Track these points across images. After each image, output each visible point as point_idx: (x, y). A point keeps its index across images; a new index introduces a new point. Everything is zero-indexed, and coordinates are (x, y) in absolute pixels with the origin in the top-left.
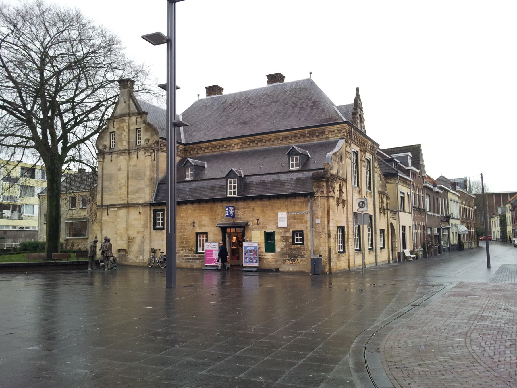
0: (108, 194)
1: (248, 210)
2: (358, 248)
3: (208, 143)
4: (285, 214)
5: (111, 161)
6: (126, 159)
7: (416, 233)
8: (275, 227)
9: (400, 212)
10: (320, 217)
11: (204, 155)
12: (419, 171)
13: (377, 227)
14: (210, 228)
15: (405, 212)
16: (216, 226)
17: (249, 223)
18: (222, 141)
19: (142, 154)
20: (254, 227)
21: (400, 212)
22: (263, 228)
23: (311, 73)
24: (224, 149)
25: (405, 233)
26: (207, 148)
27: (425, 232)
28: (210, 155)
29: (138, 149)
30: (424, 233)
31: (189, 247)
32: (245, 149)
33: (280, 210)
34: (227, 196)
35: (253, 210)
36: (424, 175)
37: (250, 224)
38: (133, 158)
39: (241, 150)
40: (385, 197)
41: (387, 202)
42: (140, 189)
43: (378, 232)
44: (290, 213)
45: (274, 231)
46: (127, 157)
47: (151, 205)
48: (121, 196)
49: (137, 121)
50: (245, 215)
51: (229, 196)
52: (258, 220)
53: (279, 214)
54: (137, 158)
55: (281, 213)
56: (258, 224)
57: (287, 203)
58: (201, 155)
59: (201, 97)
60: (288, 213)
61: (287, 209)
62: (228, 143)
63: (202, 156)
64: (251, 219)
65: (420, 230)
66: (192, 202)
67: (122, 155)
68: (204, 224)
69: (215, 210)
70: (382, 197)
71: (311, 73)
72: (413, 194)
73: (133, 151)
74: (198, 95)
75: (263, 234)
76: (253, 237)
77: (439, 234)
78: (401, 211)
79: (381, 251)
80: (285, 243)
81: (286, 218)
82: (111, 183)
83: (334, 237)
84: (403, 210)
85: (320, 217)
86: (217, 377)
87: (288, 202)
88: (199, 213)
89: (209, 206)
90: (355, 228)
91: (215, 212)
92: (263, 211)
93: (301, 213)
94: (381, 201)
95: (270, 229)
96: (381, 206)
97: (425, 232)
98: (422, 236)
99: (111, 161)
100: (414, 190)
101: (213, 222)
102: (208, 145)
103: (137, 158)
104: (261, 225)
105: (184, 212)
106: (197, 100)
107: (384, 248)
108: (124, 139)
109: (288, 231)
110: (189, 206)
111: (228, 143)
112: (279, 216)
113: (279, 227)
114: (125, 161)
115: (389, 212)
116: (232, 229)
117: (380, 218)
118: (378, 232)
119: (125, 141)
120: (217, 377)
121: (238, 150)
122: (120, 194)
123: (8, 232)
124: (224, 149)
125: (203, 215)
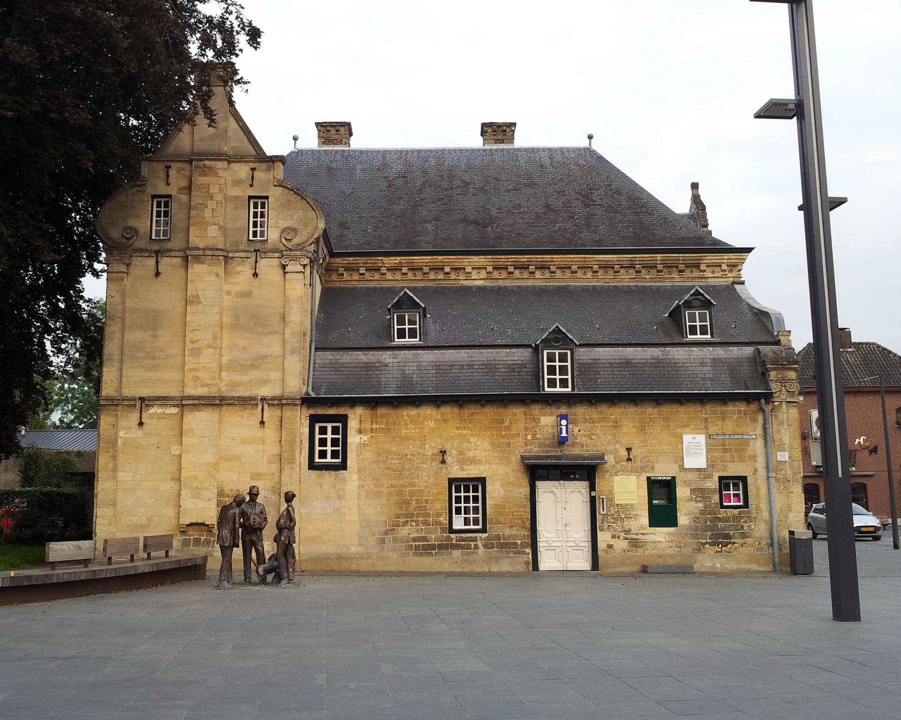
0: (142, 367)
1: (602, 426)
4: (701, 439)
5: (157, 274)
6: (217, 275)
14: (494, 467)
18: (440, 257)
22: (643, 469)
24: (441, 276)
26: (393, 269)
31: (428, 515)
32: (500, 281)
33: (687, 429)
35: (616, 425)
37: (610, 459)
38: (238, 273)
39: (488, 283)
42: (263, 357)
44: (715, 437)
46: (220, 270)
47: (307, 401)
48: (197, 374)
49: (253, 177)
50: (594, 437)
51: (548, 390)
52: (629, 450)
53: (687, 438)
54: (255, 275)
55: (692, 436)
56: (629, 459)
59: (302, 145)
60: (709, 436)
61: (706, 428)
64: (610, 448)
69: (507, 424)
76: (616, 490)
80: (700, 505)
85: (786, 447)
88: (458, 428)
89: (490, 412)
93: (740, 437)
95: (662, 472)
99: (157, 274)
103: (255, 275)
104: (638, 463)
109: (710, 477)
110: (428, 411)
112: (685, 443)
114: (214, 278)
119: (214, 224)
121: (482, 282)
122: (196, 370)
125: (472, 435)
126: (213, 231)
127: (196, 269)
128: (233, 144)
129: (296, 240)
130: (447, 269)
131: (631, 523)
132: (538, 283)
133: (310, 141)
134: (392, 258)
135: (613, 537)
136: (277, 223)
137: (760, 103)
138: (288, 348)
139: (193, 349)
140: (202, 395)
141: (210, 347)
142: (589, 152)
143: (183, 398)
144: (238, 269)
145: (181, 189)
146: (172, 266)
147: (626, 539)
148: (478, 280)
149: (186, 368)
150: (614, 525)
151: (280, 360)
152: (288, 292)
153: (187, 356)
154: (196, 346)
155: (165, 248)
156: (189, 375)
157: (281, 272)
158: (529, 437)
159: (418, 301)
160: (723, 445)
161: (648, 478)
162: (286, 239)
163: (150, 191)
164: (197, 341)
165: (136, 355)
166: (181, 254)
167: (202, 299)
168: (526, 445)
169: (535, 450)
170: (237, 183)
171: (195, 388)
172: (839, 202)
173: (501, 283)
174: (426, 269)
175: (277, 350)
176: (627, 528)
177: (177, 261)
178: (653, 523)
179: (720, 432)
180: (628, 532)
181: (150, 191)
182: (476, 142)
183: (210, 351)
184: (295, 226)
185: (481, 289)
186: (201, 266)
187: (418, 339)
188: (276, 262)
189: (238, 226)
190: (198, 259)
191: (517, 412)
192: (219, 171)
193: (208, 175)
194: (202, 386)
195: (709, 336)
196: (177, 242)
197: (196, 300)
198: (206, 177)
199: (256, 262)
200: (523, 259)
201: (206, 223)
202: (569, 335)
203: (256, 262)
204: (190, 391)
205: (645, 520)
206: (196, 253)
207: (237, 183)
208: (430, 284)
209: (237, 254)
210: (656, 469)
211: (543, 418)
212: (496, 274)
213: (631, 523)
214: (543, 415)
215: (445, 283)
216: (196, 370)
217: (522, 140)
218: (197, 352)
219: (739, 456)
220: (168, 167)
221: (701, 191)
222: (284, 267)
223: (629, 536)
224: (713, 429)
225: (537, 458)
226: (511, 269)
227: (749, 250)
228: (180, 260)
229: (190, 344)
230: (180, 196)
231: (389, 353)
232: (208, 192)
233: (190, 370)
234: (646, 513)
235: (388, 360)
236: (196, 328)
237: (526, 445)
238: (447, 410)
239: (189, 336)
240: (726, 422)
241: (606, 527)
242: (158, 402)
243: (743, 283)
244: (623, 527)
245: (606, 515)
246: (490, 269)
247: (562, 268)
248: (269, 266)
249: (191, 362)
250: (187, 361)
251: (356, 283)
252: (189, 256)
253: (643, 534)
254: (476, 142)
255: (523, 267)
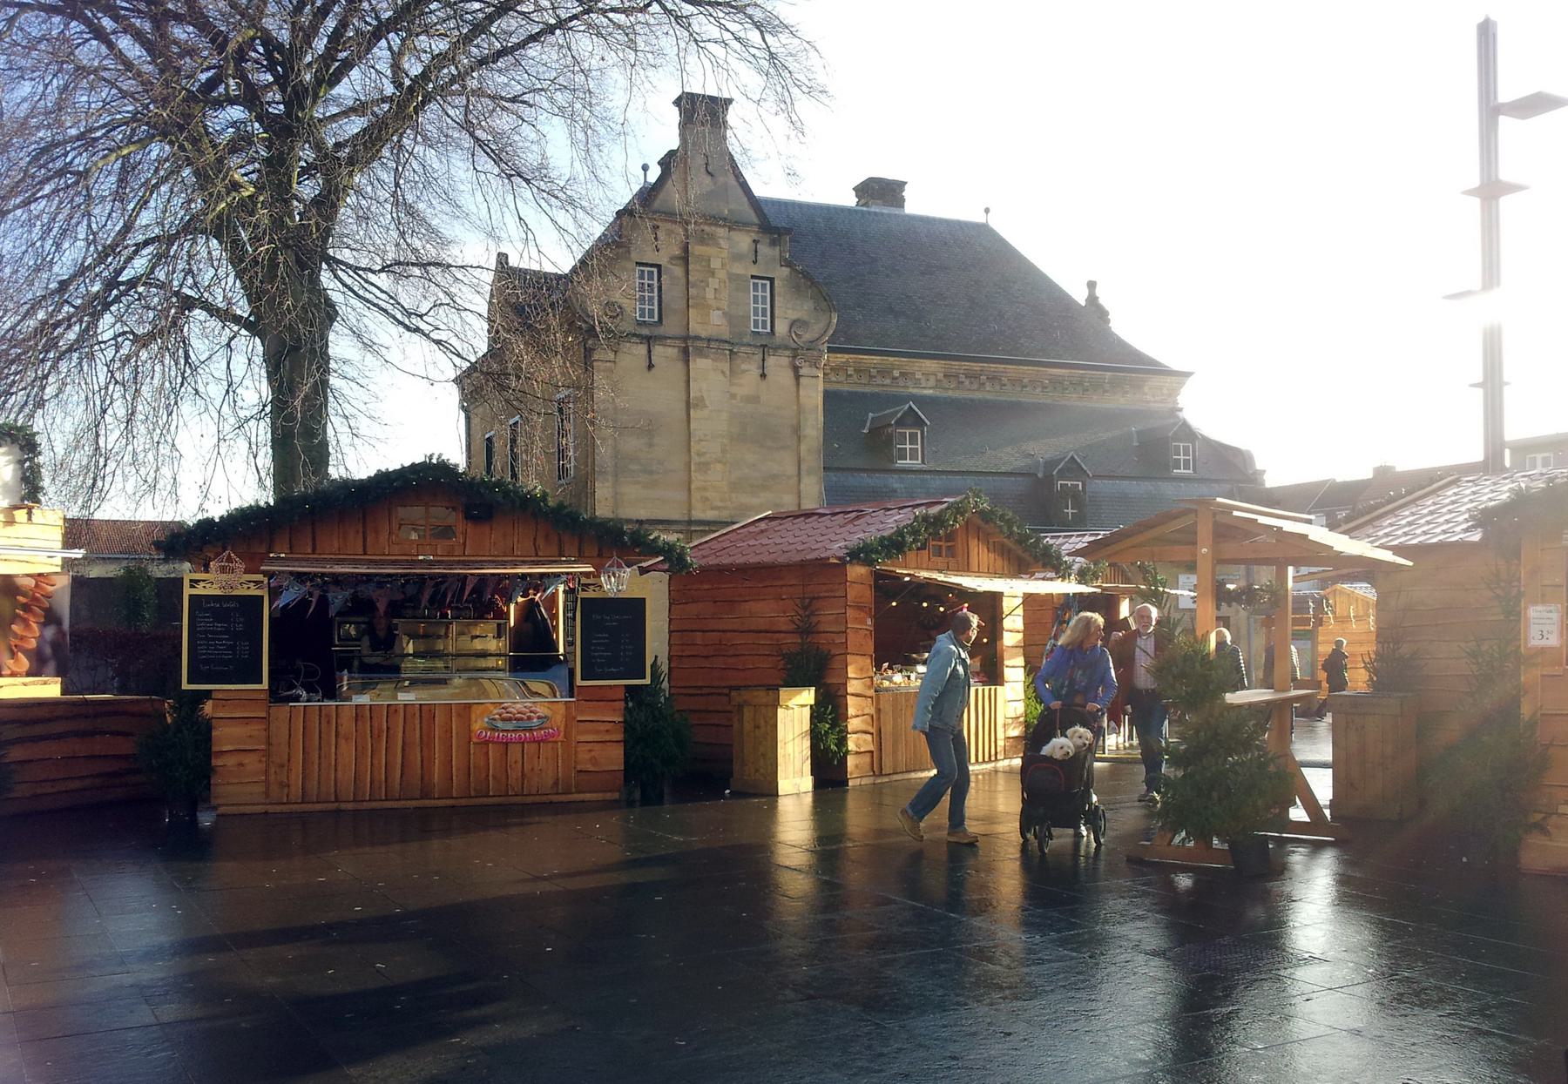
0: (639, 483)
3: (846, 356)
5: (650, 366)
6: (723, 372)
18: (891, 359)
19: (781, 366)
23: (987, 211)
24: (888, 381)
29: (766, 346)
38: (744, 372)
42: (774, 477)
46: (726, 366)
48: (708, 494)
49: (756, 252)
54: (763, 376)
55: (1187, 576)
62: (908, 369)
67: (706, 357)
71: (987, 211)
73: (749, 350)
82: (651, 445)
86: (1069, 947)
99: (650, 366)
102: (847, 361)
103: (763, 376)
108: (713, 303)
113: (1180, 607)
114: (721, 377)
119: (718, 309)
120: (1069, 947)
121: (931, 391)
122: (705, 489)
124: (888, 381)
126: (716, 318)
127: (700, 364)
128: (732, 207)
129: (808, 336)
130: (896, 373)
132: (989, 397)
134: (839, 355)
136: (785, 312)
138: (804, 467)
139: (700, 463)
140: (712, 519)
141: (719, 462)
142: (983, 230)
143: (690, 522)
144: (744, 367)
145: (673, 258)
146: (667, 357)
149: (693, 487)
151: (794, 481)
152: (802, 400)
153: (695, 471)
154: (702, 460)
155: (656, 333)
156: (696, 495)
157: (791, 374)
159: (923, 417)
162: (796, 334)
163: (635, 256)
164: (705, 453)
165: (631, 467)
166: (678, 343)
167: (707, 403)
170: (737, 257)
171: (704, 511)
172: (1507, 384)
175: (791, 469)
177: (672, 352)
181: (635, 256)
182: (850, 200)
183: (719, 467)
184: (806, 318)
186: (704, 361)
187: (920, 462)
188: (785, 361)
189: (741, 314)
190: (701, 353)
192: (721, 241)
193: (707, 245)
194: (712, 509)
195: (1191, 471)
196: (671, 327)
197: (701, 403)
198: (705, 247)
199: (763, 360)
201: (709, 306)
202: (1083, 466)
203: (763, 360)
204: (698, 514)
206: (699, 344)
207: (737, 257)
208: (877, 390)
209: (743, 349)
212: (945, 383)
216: (705, 489)
217: (915, 204)
218: (705, 467)
220: (656, 228)
221: (1099, 292)
222: (796, 369)
226: (962, 378)
227: (1188, 375)
228: (676, 350)
229: (696, 457)
230: (669, 266)
231: (896, 476)
232: (709, 266)
233: (698, 489)
235: (896, 486)
236: (702, 438)
239: (695, 447)
242: (660, 527)
243: (1181, 410)
246: (940, 376)
247: (1013, 382)
248: (778, 365)
249: (698, 479)
250: (693, 478)
252: (688, 347)
254: (850, 200)
255: (972, 376)
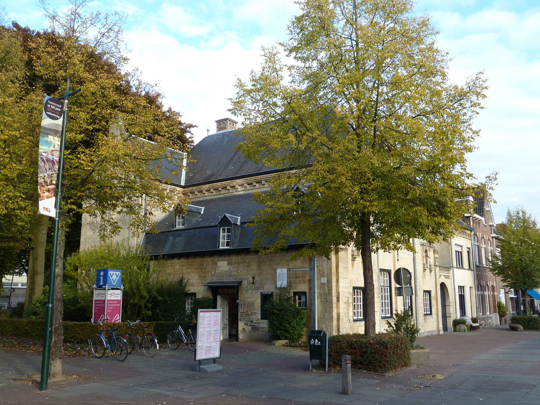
1: (242, 266)
2: (429, 313)
4: (285, 271)
7: (482, 295)
8: (273, 287)
9: (455, 269)
10: (326, 274)
11: (204, 199)
12: (483, 219)
13: (418, 287)
14: (199, 288)
15: (464, 269)
16: (205, 286)
17: (243, 282)
20: (249, 287)
21: (455, 269)
22: (259, 288)
25: (464, 296)
26: (208, 191)
27: (496, 293)
28: (210, 199)
30: (494, 296)
32: (250, 191)
33: (279, 266)
34: (219, 248)
35: (249, 265)
36: (491, 224)
37: (245, 283)
39: (246, 192)
40: (432, 250)
41: (434, 256)
43: (420, 294)
44: (292, 270)
45: (272, 293)
50: (239, 271)
51: (221, 248)
52: (253, 278)
53: (279, 271)
55: (280, 270)
56: (253, 283)
57: (288, 257)
58: (201, 199)
59: (210, 133)
60: (289, 270)
61: (288, 265)
63: (203, 201)
64: (245, 277)
65: (488, 291)
66: (179, 256)
68: (192, 283)
69: (205, 266)
70: (426, 250)
72: (477, 246)
74: (208, 131)
75: (259, 296)
77: (516, 296)
78: (457, 268)
79: (425, 320)
81: (286, 276)
83: (345, 300)
84: (460, 265)
85: (326, 274)
87: (288, 255)
88: (187, 269)
89: (198, 260)
90: (385, 289)
91: (205, 268)
92: (259, 266)
93: (303, 269)
94: (425, 254)
96: (427, 262)
97: (496, 293)
98: (491, 299)
100: (478, 241)
101: (203, 280)
104: (257, 285)
105: (171, 268)
106: (206, 136)
107: (431, 314)
110: (176, 261)
111: (231, 184)
112: (278, 273)
115: (437, 269)
116: (229, 289)
117: (424, 276)
118: (420, 294)
121: (243, 192)
123: (16, 290)
125: (192, 272)
130: (228, 188)
131: (253, 317)
133: (214, 131)
135: (245, 324)
137: (240, 78)
147: (250, 325)
148: (240, 191)
150: (246, 318)
158: (213, 273)
160: (296, 274)
161: (261, 293)
168: (212, 276)
169: (215, 279)
173: (250, 192)
174: (220, 189)
176: (251, 320)
178: (262, 318)
179: (294, 267)
180: (252, 322)
185: (240, 196)
191: (208, 260)
200: (258, 178)
205: (259, 316)
210: (265, 289)
211: (219, 262)
213: (253, 317)
214: (219, 261)
215: (228, 195)
219: (303, 280)
223: (252, 324)
224: (291, 265)
225: (219, 282)
234: (259, 312)
237: (212, 276)
238: (183, 260)
240: (297, 260)
241: (242, 319)
244: (249, 319)
245: (243, 312)
251: (194, 199)
253: (258, 323)
